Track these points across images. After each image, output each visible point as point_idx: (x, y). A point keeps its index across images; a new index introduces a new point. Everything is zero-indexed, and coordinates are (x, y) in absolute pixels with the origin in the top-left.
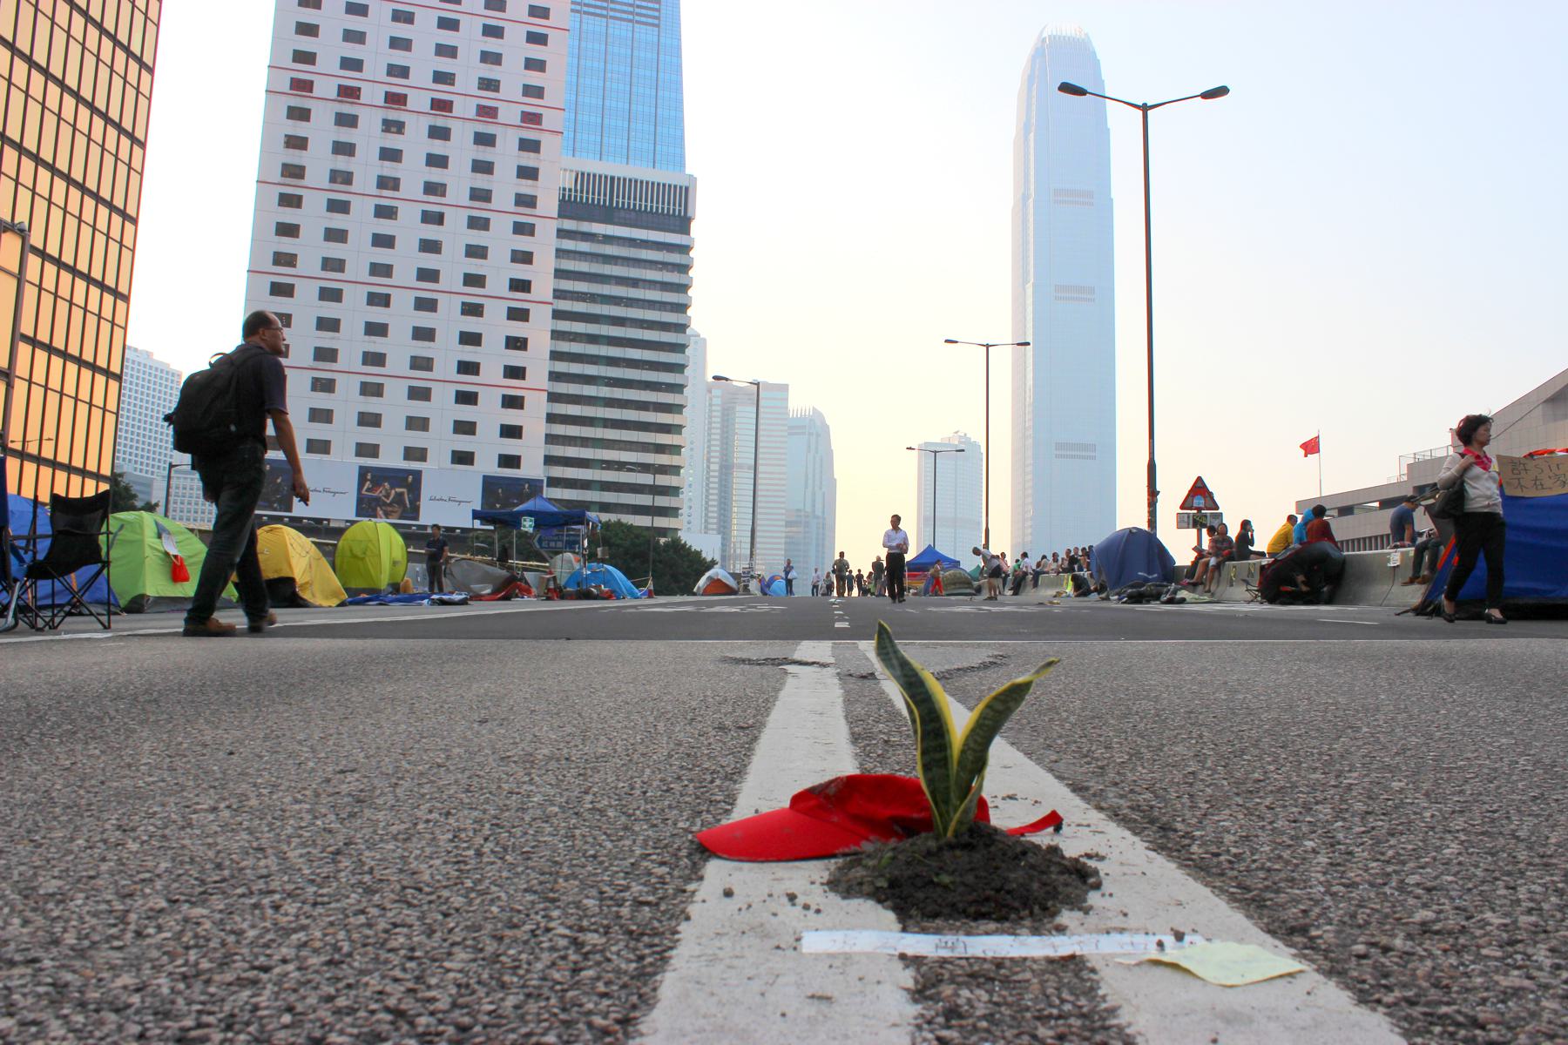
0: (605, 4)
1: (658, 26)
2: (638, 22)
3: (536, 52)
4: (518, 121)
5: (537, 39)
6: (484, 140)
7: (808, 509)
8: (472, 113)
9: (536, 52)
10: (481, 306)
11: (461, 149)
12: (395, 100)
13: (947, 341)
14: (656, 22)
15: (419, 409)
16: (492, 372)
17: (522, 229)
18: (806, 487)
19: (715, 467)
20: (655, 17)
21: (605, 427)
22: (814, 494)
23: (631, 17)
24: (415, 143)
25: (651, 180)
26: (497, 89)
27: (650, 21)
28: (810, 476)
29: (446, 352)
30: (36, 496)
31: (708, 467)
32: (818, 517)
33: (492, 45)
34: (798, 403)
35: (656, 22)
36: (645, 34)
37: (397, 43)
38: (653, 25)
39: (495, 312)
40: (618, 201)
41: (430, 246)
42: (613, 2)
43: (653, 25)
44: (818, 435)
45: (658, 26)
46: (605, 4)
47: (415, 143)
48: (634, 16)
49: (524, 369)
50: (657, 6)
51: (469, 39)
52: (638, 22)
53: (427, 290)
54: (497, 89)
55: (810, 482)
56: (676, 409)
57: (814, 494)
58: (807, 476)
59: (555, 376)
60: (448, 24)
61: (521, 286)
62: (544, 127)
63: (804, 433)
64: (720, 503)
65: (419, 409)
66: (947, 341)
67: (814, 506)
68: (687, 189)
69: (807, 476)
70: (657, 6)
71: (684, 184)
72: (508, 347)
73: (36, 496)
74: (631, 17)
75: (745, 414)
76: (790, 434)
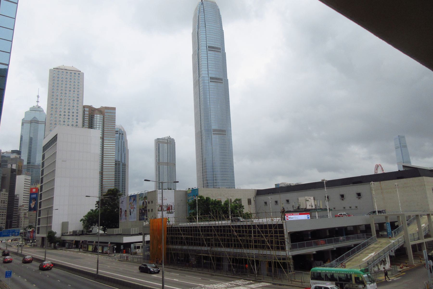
63: (118, 133)
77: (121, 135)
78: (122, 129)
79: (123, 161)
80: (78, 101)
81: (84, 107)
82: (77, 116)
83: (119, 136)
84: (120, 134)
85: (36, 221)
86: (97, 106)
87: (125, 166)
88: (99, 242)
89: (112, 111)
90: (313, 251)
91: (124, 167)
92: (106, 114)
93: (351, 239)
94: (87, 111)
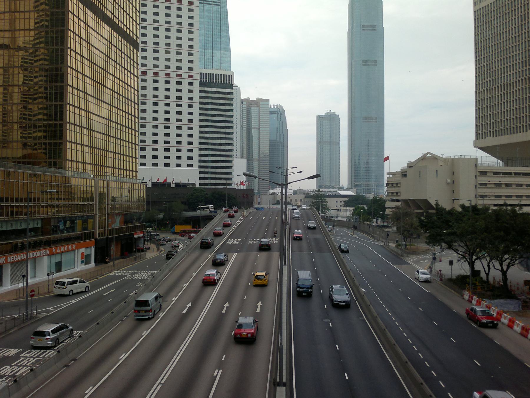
0: (203, 2)
1: (220, 5)
2: (213, 4)
3: (191, 58)
5: (191, 54)
6: (179, 83)
7: (278, 140)
8: (175, 76)
9: (191, 58)
10: (181, 127)
11: (173, 86)
12: (156, 74)
13: (301, 172)
14: (219, 4)
16: (184, 143)
17: (190, 106)
19: (245, 129)
20: (219, 2)
21: (211, 145)
23: (211, 3)
25: (223, 74)
27: (217, 4)
31: (242, 129)
33: (179, 13)
34: (273, 103)
35: (219, 4)
36: (216, 8)
39: (185, 128)
40: (212, 80)
41: (167, 112)
42: (205, 1)
44: (281, 114)
45: (220, 5)
46: (203, 2)
48: (212, 4)
49: (165, 113)
50: (219, 1)
51: (162, 10)
52: (213, 4)
53: (167, 123)
55: (278, 130)
56: (231, 110)
57: (280, 135)
59: (200, 144)
60: (156, 7)
61: (190, 121)
62: (194, 79)
63: (276, 114)
64: (247, 115)
66: (301, 172)
67: (280, 139)
68: (231, 76)
70: (219, 1)
71: (231, 74)
72: (165, 61)
74: (211, 3)
75: (254, 110)
76: (270, 114)
77: (279, 115)
78: (280, 108)
79: (282, 140)
80: (237, 133)
81: (242, 101)
82: (236, 123)
83: (278, 116)
84: (278, 114)
85: (441, 286)
86: (253, 98)
87: (283, 147)
88: (28, 231)
89: (266, 103)
90: (513, 183)
91: (283, 148)
92: (261, 106)
93: (51, 244)
94: (245, 130)
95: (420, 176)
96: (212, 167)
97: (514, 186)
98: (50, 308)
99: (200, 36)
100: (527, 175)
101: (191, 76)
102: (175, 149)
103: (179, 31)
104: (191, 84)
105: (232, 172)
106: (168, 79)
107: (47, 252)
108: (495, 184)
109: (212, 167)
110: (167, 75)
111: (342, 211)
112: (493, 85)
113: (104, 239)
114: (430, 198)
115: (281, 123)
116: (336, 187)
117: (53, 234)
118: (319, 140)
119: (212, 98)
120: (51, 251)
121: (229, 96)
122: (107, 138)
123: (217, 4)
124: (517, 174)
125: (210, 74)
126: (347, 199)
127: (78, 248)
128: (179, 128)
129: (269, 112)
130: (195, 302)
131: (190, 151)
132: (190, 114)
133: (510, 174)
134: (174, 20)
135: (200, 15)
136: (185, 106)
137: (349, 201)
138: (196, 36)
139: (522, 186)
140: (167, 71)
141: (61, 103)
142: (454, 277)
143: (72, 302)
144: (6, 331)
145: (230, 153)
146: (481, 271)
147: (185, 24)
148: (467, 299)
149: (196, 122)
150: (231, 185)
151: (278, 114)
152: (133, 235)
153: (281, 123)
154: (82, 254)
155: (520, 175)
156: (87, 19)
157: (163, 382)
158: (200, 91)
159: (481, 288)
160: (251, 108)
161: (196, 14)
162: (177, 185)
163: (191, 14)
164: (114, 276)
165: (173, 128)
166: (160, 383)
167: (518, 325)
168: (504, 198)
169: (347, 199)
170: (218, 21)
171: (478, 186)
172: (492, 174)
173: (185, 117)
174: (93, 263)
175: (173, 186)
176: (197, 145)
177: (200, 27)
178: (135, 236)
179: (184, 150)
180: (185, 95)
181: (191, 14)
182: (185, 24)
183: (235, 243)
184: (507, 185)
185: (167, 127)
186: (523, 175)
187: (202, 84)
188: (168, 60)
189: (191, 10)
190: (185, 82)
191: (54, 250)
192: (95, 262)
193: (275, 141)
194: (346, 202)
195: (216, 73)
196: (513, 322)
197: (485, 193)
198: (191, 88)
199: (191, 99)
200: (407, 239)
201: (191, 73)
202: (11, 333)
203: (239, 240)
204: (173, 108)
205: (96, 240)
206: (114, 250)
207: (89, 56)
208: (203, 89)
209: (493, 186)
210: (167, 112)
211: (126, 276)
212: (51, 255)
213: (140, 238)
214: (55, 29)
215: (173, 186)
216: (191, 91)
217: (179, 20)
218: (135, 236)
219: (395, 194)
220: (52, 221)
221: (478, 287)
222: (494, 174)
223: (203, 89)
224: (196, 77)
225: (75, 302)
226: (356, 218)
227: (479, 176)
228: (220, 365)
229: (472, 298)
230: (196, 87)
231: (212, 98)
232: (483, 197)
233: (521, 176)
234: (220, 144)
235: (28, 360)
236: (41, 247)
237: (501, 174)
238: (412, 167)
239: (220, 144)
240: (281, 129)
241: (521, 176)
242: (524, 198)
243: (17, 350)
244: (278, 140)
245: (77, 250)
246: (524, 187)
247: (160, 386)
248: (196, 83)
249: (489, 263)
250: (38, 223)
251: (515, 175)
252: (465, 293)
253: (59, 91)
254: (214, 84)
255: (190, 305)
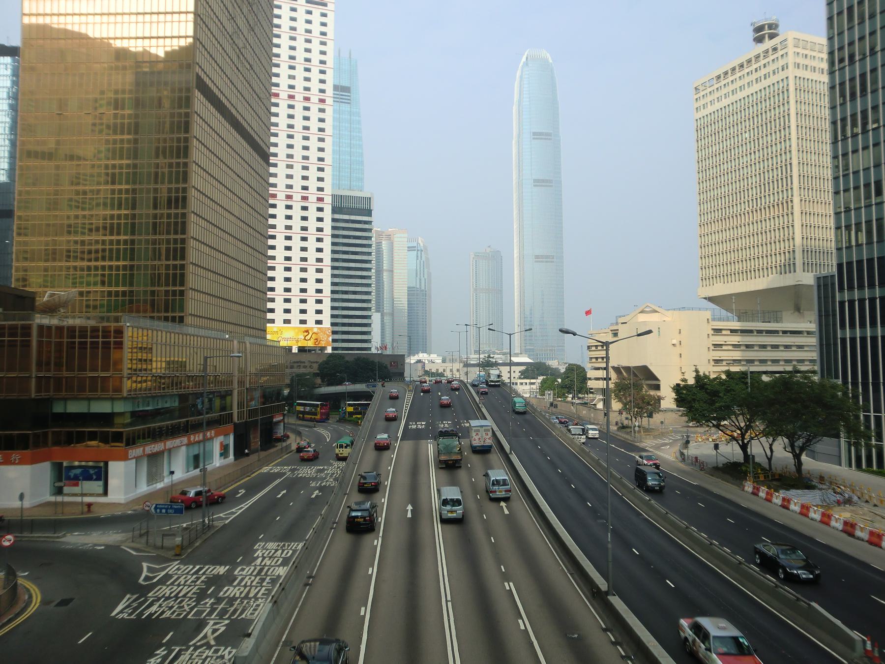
4: (316, 201)
7: (418, 286)
15: (287, 306)
16: (311, 291)
18: (417, 276)
20: (348, 100)
22: (420, 280)
24: (300, 55)
25: (356, 196)
26: (307, 230)
28: (419, 270)
29: (296, 243)
30: (162, 545)
32: (422, 291)
33: (307, 113)
37: (293, 77)
38: (349, 103)
40: (345, 205)
41: (288, 248)
43: (349, 103)
47: (300, 55)
49: (317, 251)
50: (349, 94)
54: (307, 230)
55: (419, 273)
58: (417, 271)
65: (288, 274)
69: (417, 271)
70: (349, 94)
71: (369, 196)
73: (162, 545)
76: (408, 250)
77: (419, 252)
83: (417, 253)
84: (418, 250)
95: (659, 335)
96: (344, 325)
97: (756, 348)
98: (221, 515)
99: (333, 145)
100: (771, 333)
101: (320, 200)
102: (282, 299)
103: (306, 138)
104: (320, 210)
105: (370, 332)
106: (289, 203)
107: (185, 440)
108: (733, 345)
109: (344, 325)
110: (289, 197)
111: (518, 384)
112: (722, 215)
113: (242, 422)
114: (651, 364)
115: (422, 262)
116: (499, 352)
117: (191, 417)
118: (474, 287)
119: (344, 229)
120: (189, 439)
121: (366, 226)
122: (233, 284)
123: (346, 101)
124: (760, 332)
125: (341, 196)
126: (523, 368)
127: (217, 435)
128: (304, 270)
129: (407, 249)
130: (414, 501)
131: (319, 302)
132: (319, 250)
133: (751, 331)
134: (299, 123)
135: (334, 118)
136: (312, 239)
137: (527, 370)
138: (328, 145)
139: (778, 348)
140: (289, 192)
141: (183, 237)
142: (721, 465)
143: (242, 508)
144: (190, 544)
145: (368, 305)
146: (756, 456)
147: (314, 129)
148: (751, 492)
149: (327, 261)
150: (370, 349)
151: (418, 250)
152: (272, 417)
153: (422, 262)
154: (221, 443)
155: (762, 333)
156: (214, 123)
157: (449, 598)
158: (334, 220)
159: (765, 476)
160: (381, 242)
161: (329, 115)
162: (302, 350)
163: (322, 115)
164: (268, 474)
165: (296, 269)
166: (447, 601)
167: (837, 520)
168: (782, 363)
169: (523, 368)
170: (347, 125)
171: (712, 348)
172: (729, 333)
173: (312, 255)
174: (231, 457)
175: (295, 350)
176: (329, 294)
177: (334, 134)
178: (274, 420)
179: (311, 301)
180: (312, 224)
181: (322, 115)
182: (314, 129)
183: (419, 427)
184: (786, 347)
185: (288, 269)
186: (766, 333)
187: (335, 210)
188: (290, 177)
189: (322, 110)
190: (313, 208)
191: (192, 439)
192: (235, 455)
193: (414, 288)
194: (522, 372)
195: (347, 194)
196: (829, 517)
197: (720, 357)
198: (320, 215)
199: (320, 230)
200: (636, 418)
201: (320, 194)
202: (197, 547)
203: (424, 423)
204: (296, 243)
205: (235, 424)
206: (256, 440)
207: (215, 172)
208: (337, 216)
209: (730, 348)
210: (288, 248)
211: (285, 474)
212: (189, 444)
213: (279, 422)
214: (175, 136)
215: (295, 350)
216: (320, 220)
217: (306, 123)
218: (274, 420)
219: (600, 360)
220: (190, 397)
221: (760, 475)
222: (731, 332)
223: (337, 216)
224: (328, 200)
225: (246, 507)
226: (549, 393)
227: (712, 335)
228: (506, 577)
229: (758, 489)
230: (327, 214)
231: (344, 229)
232: (717, 361)
233: (764, 334)
234: (355, 293)
235: (170, 589)
236: (179, 433)
237: (739, 332)
238: (626, 323)
239: (355, 293)
240: (422, 271)
241: (764, 334)
242: (769, 363)
243: (223, 567)
244: (418, 286)
245: (215, 439)
246: (769, 348)
247: (450, 604)
248: (328, 209)
249: (771, 445)
250: (175, 401)
251: (783, 333)
252: (746, 484)
253: (179, 220)
254: (346, 209)
255: (410, 507)
